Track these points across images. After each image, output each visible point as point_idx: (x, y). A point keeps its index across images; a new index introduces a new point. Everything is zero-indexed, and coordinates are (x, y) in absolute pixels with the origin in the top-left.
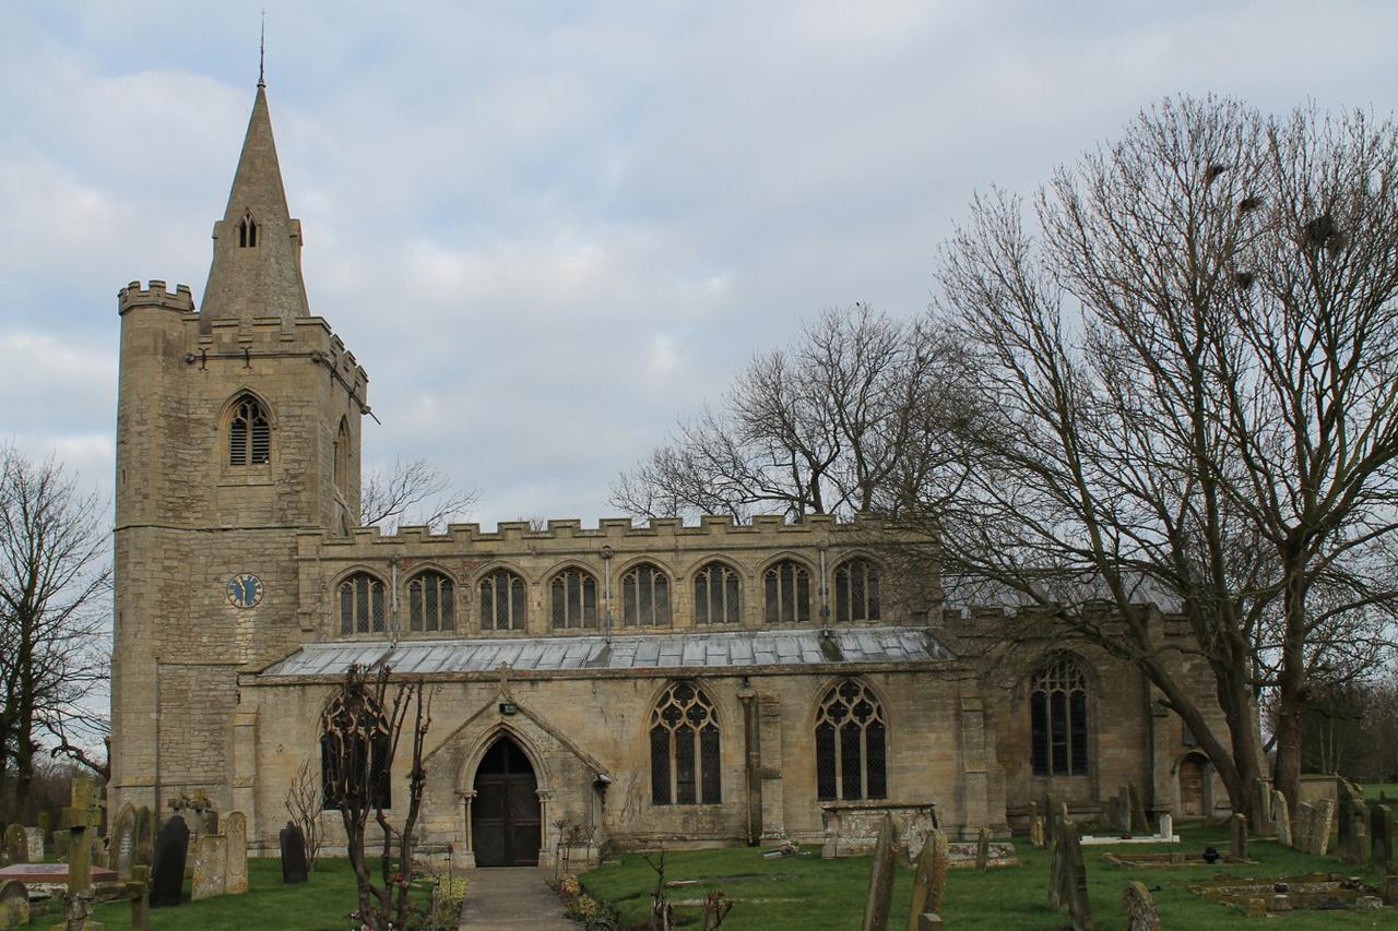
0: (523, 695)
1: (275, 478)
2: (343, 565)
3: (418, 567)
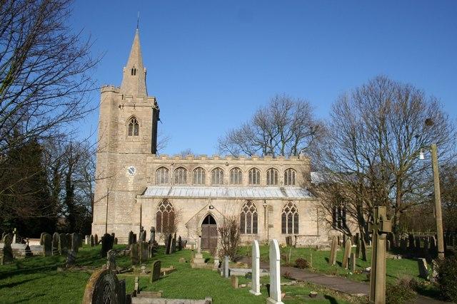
0: (214, 203)
3: (178, 166)
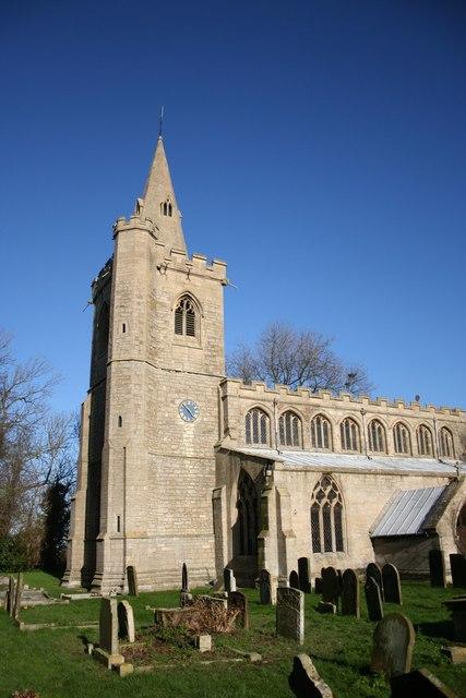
3: (286, 408)
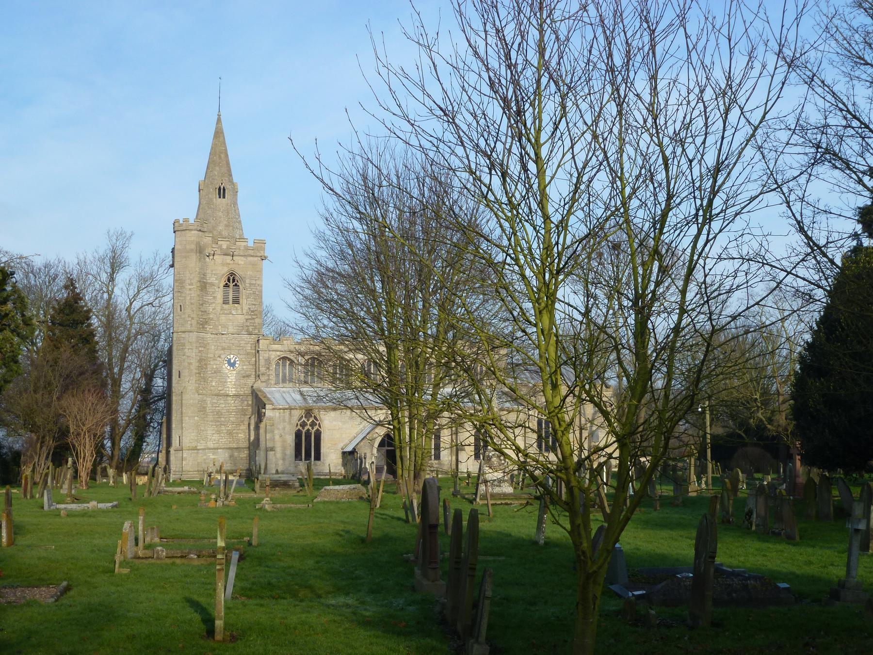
1: (244, 312)
2: (278, 353)
